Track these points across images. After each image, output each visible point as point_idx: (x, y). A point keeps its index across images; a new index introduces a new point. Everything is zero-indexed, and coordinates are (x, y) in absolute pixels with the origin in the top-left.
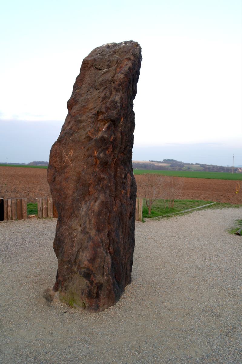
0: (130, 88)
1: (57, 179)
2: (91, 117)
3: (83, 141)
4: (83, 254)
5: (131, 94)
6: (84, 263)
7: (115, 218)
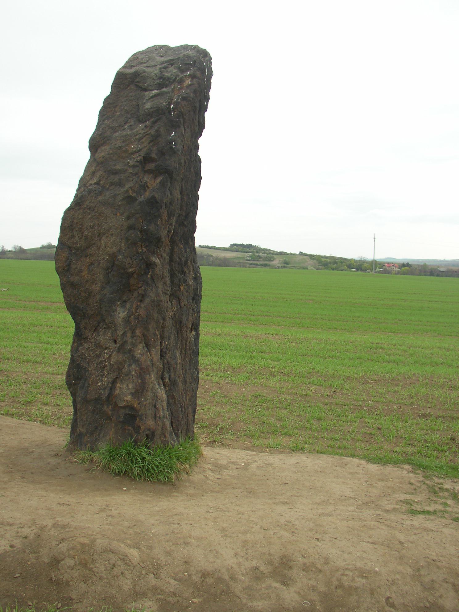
0: (195, 121)
1: (73, 267)
2: (134, 166)
3: (120, 203)
4: (123, 385)
5: (197, 129)
6: (125, 398)
7: (170, 330)
